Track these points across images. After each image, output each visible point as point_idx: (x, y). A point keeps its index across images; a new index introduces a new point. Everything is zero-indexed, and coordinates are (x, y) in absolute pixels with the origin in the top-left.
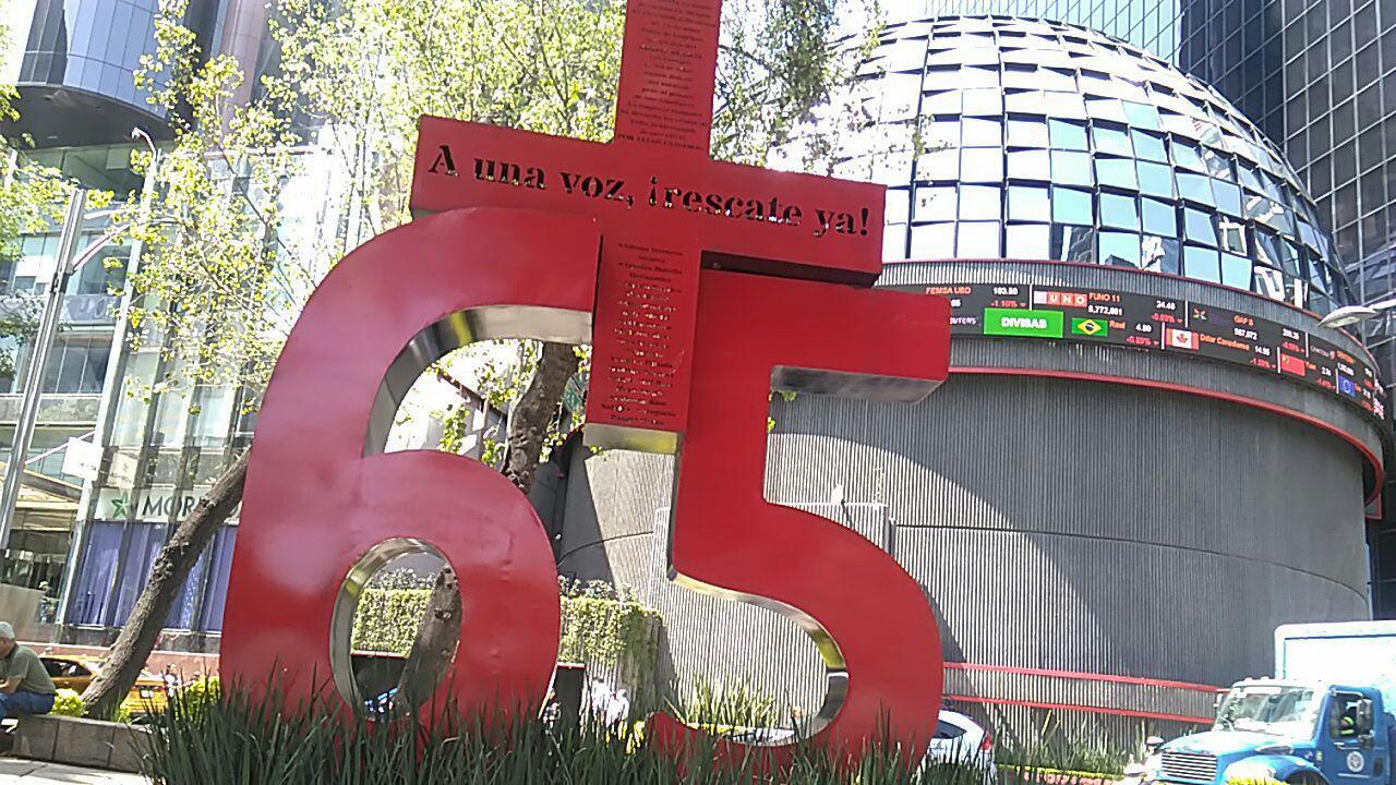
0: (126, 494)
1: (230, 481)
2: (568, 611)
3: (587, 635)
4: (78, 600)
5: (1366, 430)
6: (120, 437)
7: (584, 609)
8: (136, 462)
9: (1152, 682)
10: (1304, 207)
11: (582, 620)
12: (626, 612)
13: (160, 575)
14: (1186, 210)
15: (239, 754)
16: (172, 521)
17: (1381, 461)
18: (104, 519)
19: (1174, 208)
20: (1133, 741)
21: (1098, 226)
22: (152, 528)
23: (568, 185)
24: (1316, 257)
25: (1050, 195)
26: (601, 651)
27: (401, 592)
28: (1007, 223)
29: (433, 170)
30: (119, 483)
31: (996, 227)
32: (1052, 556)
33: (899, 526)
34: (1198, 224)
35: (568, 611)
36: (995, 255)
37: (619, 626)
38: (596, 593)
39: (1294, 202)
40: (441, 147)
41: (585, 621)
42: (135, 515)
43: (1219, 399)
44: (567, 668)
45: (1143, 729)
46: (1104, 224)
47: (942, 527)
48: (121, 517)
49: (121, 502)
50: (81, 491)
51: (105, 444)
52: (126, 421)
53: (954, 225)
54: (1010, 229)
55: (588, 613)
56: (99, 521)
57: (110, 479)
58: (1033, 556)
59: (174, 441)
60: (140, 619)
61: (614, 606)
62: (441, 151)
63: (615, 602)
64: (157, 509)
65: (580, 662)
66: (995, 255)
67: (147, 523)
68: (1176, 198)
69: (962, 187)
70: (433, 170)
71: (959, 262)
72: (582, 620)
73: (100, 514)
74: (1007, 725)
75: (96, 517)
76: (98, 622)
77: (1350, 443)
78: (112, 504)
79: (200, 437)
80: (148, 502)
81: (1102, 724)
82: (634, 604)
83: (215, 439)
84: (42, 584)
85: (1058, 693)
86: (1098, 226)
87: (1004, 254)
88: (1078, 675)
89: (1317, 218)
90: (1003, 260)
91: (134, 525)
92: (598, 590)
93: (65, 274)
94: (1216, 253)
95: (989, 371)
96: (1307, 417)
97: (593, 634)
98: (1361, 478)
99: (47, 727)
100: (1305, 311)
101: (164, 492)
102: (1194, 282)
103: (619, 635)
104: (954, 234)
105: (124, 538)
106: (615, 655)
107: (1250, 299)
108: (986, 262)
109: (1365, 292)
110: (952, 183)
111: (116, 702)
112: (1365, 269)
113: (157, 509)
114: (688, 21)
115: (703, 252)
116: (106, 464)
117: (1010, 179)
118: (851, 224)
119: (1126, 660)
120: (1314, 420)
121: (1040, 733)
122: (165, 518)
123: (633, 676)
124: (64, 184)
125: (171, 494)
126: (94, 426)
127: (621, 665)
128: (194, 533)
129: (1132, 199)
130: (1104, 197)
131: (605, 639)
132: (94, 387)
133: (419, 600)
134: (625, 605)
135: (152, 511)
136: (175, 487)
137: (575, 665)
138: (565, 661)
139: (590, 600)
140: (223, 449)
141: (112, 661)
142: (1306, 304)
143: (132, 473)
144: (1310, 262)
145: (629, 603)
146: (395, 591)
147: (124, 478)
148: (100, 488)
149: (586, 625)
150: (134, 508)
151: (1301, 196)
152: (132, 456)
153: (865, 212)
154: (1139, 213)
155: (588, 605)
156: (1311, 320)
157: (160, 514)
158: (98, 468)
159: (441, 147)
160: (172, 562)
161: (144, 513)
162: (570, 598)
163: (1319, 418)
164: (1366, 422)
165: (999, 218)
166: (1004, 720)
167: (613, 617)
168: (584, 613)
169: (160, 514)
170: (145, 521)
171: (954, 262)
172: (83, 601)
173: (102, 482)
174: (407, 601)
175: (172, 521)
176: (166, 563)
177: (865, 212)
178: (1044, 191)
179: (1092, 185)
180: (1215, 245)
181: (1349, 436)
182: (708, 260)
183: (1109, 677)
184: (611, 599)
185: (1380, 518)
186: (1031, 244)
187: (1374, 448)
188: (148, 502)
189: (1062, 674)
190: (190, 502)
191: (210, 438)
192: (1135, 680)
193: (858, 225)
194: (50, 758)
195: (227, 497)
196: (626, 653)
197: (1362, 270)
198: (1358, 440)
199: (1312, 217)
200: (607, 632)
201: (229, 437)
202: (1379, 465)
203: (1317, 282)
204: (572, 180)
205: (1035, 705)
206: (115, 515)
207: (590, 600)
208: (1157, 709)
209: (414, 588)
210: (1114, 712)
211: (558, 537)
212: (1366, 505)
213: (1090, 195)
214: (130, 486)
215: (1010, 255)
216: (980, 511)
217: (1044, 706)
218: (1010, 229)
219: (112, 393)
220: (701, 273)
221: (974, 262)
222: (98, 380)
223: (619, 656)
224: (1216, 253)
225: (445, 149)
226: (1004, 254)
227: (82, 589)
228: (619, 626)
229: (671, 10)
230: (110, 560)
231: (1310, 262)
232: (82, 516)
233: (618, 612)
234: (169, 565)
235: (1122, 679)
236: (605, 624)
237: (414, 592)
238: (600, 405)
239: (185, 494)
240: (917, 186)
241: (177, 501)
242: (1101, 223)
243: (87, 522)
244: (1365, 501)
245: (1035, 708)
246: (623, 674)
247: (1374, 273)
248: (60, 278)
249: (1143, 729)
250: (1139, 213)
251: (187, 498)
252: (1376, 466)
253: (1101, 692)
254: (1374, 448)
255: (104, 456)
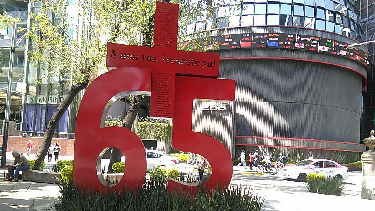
0: (34, 96)
1: (64, 104)
2: (152, 126)
3: (157, 132)
4: (25, 125)
5: (363, 69)
6: (30, 80)
7: (156, 126)
8: (36, 88)
9: (302, 139)
10: (350, 5)
11: (156, 128)
12: (167, 126)
13: (49, 129)
14: (317, 9)
15: (83, 206)
16: (47, 104)
17: (367, 78)
18: (29, 103)
19: (314, 9)
20: (296, 154)
21: (293, 15)
22: (42, 106)
23: (143, 58)
24: (353, 21)
25: (280, 6)
26: (161, 136)
27: (109, 122)
28: (267, 14)
29: (111, 57)
30: (31, 93)
31: (265, 16)
32: (277, 108)
33: (238, 101)
34: (320, 13)
35: (152, 126)
36: (264, 24)
37: (165, 130)
38: (159, 121)
39: (348, 5)
40: (113, 51)
41: (157, 129)
42: (37, 102)
43: (323, 63)
44: (153, 141)
45: (299, 151)
46: (294, 14)
47: (249, 101)
48: (33, 103)
49: (33, 99)
50: (22, 99)
51: (27, 83)
52: (31, 76)
53: (253, 15)
54: (268, 16)
55: (157, 127)
56: (28, 104)
57: (29, 93)
58: (272, 108)
59: (45, 82)
60: (45, 140)
61: (164, 125)
62: (113, 52)
63: (164, 124)
64: (43, 100)
65: (156, 139)
66: (264, 24)
67: (40, 104)
68: (314, 6)
69: (255, 4)
70: (111, 57)
71: (254, 27)
72: (156, 128)
73: (28, 102)
74: (264, 151)
75: (27, 103)
76: (31, 131)
77: (359, 74)
78: (31, 99)
79: (52, 81)
80: (40, 98)
81: (288, 150)
82: (169, 124)
83: (56, 81)
84: (15, 119)
85: (277, 143)
86: (293, 15)
87: (266, 24)
88: (283, 138)
89: (354, 8)
90: (266, 26)
91: (37, 105)
92: (159, 120)
93: (14, 48)
94: (325, 21)
95: (262, 58)
96: (347, 67)
97: (159, 132)
98: (361, 82)
99: (29, 173)
100: (348, 37)
101: (44, 96)
102: (318, 30)
103: (165, 132)
104: (253, 18)
105: (35, 108)
106: (164, 137)
107: (333, 35)
108: (261, 27)
109: (368, 27)
110: (253, 3)
111: (42, 161)
112: (368, 20)
113: (43, 100)
114: (171, 14)
115: (176, 74)
116: (28, 88)
117: (269, 2)
118: (211, 64)
119: (295, 134)
120: (349, 68)
121: (273, 153)
122: (45, 103)
123: (169, 142)
124: (8, 16)
125: (46, 97)
126: (23, 76)
127: (166, 140)
128: (56, 118)
129: (302, 6)
130: (295, 6)
131: (162, 133)
132: (21, 65)
133: (113, 124)
134: (167, 124)
135: (41, 101)
136: (47, 95)
137: (154, 140)
138: (152, 139)
139: (157, 123)
140: (58, 84)
141: (40, 151)
142: (349, 35)
143: (35, 91)
144: (351, 22)
145: (167, 124)
146: (107, 122)
147: (33, 92)
148: (27, 95)
149: (157, 130)
150: (36, 100)
151: (350, 2)
152: (34, 86)
153: (214, 61)
154: (304, 11)
155: (157, 125)
156: (350, 40)
157: (43, 102)
158: (26, 90)
159: (113, 51)
160: (52, 125)
161: (39, 101)
162: (153, 123)
163: (350, 67)
164: (363, 67)
165: (265, 13)
166: (264, 150)
167: (164, 128)
168: (156, 127)
169: (43, 102)
170: (40, 104)
171: (253, 27)
172: (26, 125)
173: (27, 93)
174: (110, 124)
175: (47, 104)
176: (50, 126)
177: (214, 61)
178: (278, 5)
179: (291, 3)
180: (325, 19)
181: (358, 72)
182: (177, 75)
183: (291, 139)
184: (163, 123)
185: (366, 91)
186: (274, 21)
187: (365, 74)
188: (40, 98)
189: (278, 138)
190: (51, 98)
191: (54, 81)
192: (297, 139)
193: (213, 65)
194: (31, 180)
195: (63, 108)
196: (167, 137)
197: (367, 21)
198: (361, 73)
199: (353, 8)
200: (162, 132)
201: (59, 80)
202: (366, 79)
203: (352, 28)
204: (144, 57)
205: (271, 146)
206: (32, 102)
207: (157, 123)
208: (302, 146)
209: (112, 121)
210: (292, 147)
211: (149, 104)
212: (362, 89)
213: (290, 6)
214: (35, 94)
215: (268, 24)
216: (258, 96)
217: (274, 146)
218: (268, 16)
219: (27, 67)
220: (176, 77)
221: (258, 27)
222: (22, 63)
223: (166, 137)
224: (325, 21)
225: (114, 51)
226: (266, 24)
227: (26, 122)
228: (165, 130)
229: (166, 11)
230: (32, 114)
231: (351, 22)
232: (23, 102)
233: (165, 126)
234: (51, 126)
235: (294, 139)
236: (162, 129)
237: (112, 122)
238: (154, 113)
239: (49, 96)
240: (243, 4)
241: (48, 98)
242: (293, 14)
243: (25, 104)
244: (362, 88)
245: (272, 147)
246: (167, 142)
247: (371, 21)
248: (13, 49)
249: (299, 151)
250: (304, 11)
251: (50, 97)
252: (365, 79)
253: (288, 143)
254: (365, 74)
255: (27, 86)
